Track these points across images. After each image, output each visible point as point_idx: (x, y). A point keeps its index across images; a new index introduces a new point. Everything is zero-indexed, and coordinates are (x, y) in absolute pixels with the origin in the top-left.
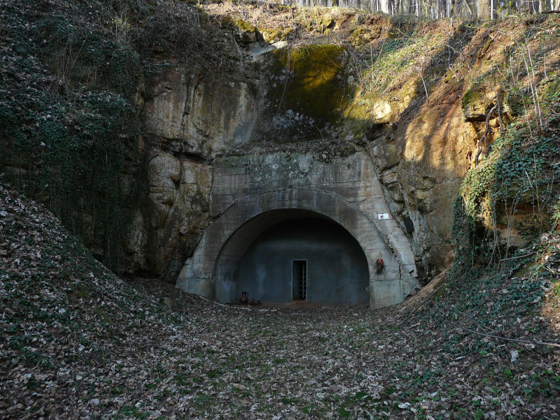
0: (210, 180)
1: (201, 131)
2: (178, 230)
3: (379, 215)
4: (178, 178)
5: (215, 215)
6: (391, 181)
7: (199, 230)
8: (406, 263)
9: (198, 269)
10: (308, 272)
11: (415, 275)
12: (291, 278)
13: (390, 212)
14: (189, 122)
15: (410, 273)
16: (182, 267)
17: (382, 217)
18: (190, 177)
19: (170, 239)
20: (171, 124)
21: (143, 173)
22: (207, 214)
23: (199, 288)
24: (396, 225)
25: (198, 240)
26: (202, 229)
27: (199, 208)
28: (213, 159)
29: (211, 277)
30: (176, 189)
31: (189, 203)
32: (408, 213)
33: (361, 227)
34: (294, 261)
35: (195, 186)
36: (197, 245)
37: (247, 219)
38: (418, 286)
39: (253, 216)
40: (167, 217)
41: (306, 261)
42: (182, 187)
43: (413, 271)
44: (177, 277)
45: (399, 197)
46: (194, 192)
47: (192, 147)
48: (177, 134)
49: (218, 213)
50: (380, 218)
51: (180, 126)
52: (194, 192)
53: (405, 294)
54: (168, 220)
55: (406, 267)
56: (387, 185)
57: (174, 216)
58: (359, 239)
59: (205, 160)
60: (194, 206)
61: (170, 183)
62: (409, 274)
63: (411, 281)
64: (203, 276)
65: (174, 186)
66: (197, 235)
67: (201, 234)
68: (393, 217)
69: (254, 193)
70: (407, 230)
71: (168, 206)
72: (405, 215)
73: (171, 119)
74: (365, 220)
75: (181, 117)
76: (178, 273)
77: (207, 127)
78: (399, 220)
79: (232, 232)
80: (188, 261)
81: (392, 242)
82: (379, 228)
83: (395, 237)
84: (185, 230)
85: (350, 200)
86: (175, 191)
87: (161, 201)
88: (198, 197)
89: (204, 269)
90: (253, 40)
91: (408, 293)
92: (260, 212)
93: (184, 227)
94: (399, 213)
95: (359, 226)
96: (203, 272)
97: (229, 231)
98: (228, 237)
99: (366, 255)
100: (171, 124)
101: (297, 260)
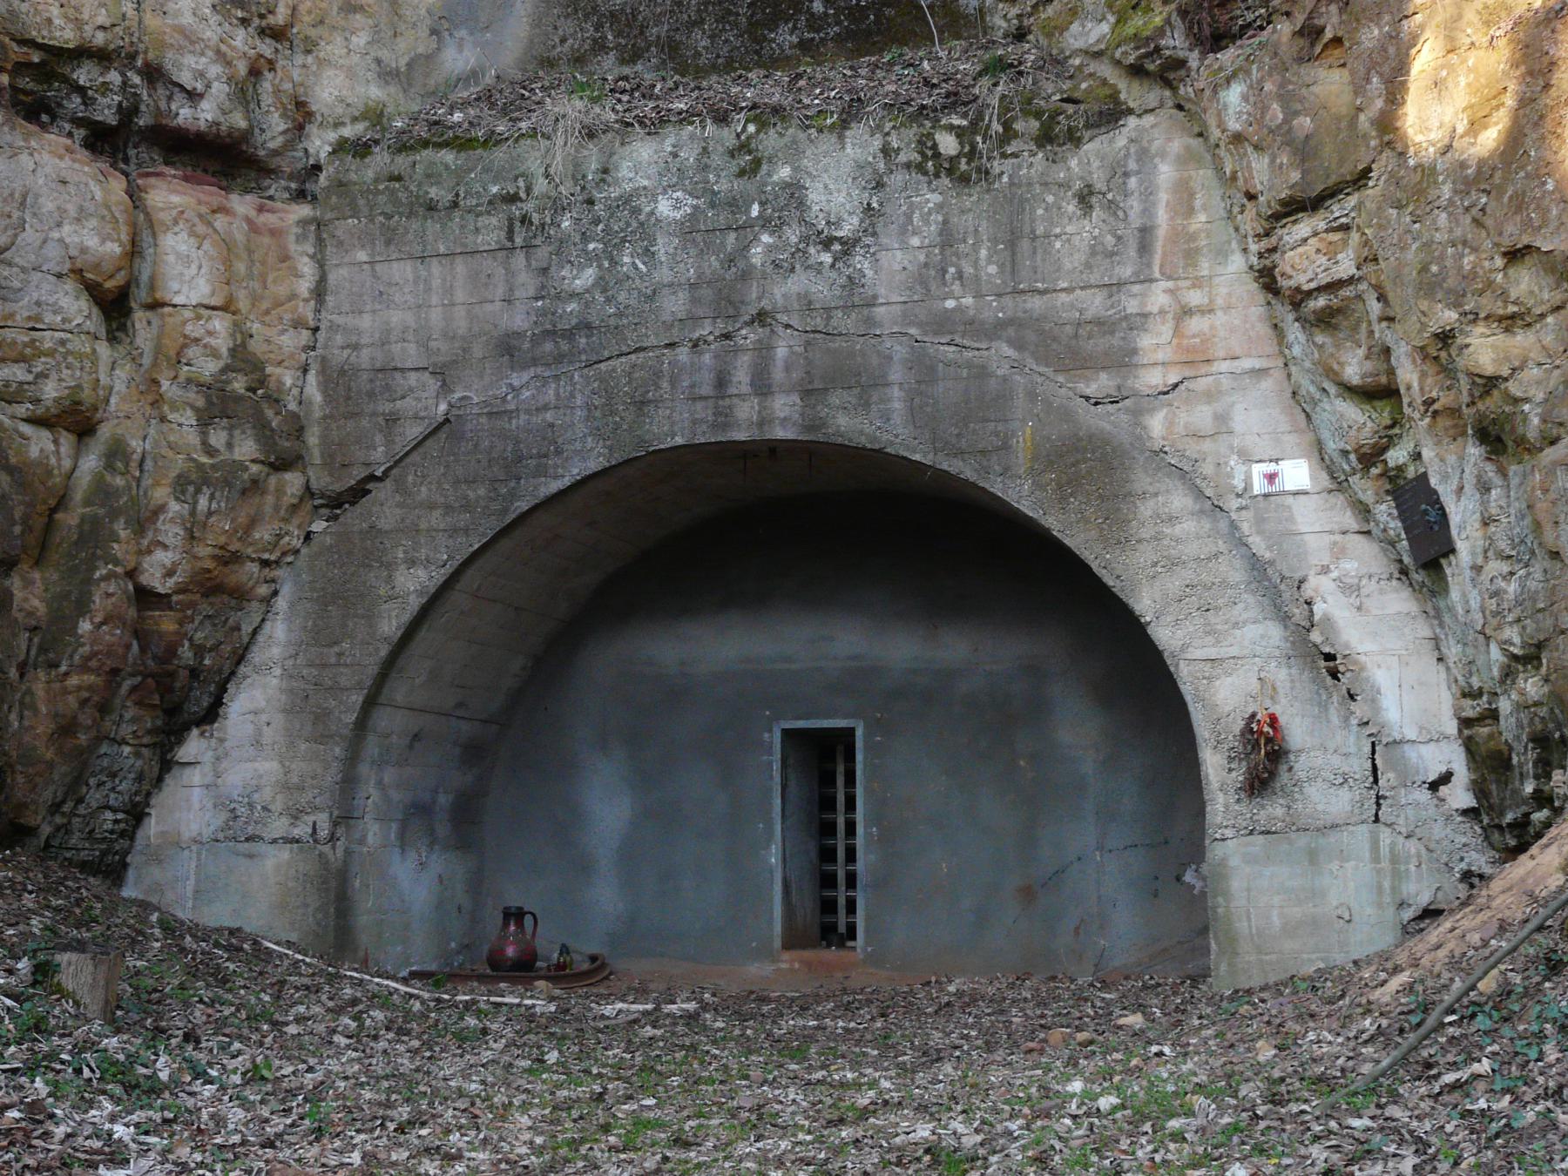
0: (304, 286)
2: (131, 574)
3: (1258, 470)
5: (338, 487)
7: (254, 568)
8: (1411, 734)
11: (1460, 796)
15: (1434, 786)
17: (1271, 478)
18: (186, 270)
19: (85, 626)
22: (293, 482)
24: (1349, 520)
25: (247, 629)
26: (265, 563)
28: (317, 168)
29: (323, 833)
30: (112, 339)
32: (1417, 456)
33: (1157, 538)
34: (786, 733)
35: (220, 324)
36: (240, 657)
37: (523, 505)
38: (1479, 860)
39: (555, 486)
40: (62, 502)
41: (850, 732)
43: (1446, 778)
44: (129, 834)
45: (1369, 366)
46: (215, 354)
47: (193, 96)
48: (102, 19)
49: (359, 473)
50: (1259, 486)
52: (215, 354)
53: (1402, 905)
55: (1411, 753)
57: (101, 491)
60: (217, 438)
61: (75, 306)
62: (1424, 795)
63: (1438, 831)
64: (279, 826)
65: (95, 323)
66: (240, 596)
69: (559, 358)
71: (67, 440)
72: (1400, 469)
76: (137, 814)
78: (1368, 497)
80: (193, 746)
81: (1327, 619)
82: (1258, 544)
83: (1349, 588)
84: (170, 573)
85: (1091, 390)
86: (103, 349)
87: (22, 410)
88: (239, 385)
89: (286, 787)
91: (1424, 899)
92: (594, 464)
93: (163, 557)
94: (1370, 457)
95: (1145, 533)
96: (277, 806)
97: (421, 573)
99: (1186, 689)
101: (801, 724)
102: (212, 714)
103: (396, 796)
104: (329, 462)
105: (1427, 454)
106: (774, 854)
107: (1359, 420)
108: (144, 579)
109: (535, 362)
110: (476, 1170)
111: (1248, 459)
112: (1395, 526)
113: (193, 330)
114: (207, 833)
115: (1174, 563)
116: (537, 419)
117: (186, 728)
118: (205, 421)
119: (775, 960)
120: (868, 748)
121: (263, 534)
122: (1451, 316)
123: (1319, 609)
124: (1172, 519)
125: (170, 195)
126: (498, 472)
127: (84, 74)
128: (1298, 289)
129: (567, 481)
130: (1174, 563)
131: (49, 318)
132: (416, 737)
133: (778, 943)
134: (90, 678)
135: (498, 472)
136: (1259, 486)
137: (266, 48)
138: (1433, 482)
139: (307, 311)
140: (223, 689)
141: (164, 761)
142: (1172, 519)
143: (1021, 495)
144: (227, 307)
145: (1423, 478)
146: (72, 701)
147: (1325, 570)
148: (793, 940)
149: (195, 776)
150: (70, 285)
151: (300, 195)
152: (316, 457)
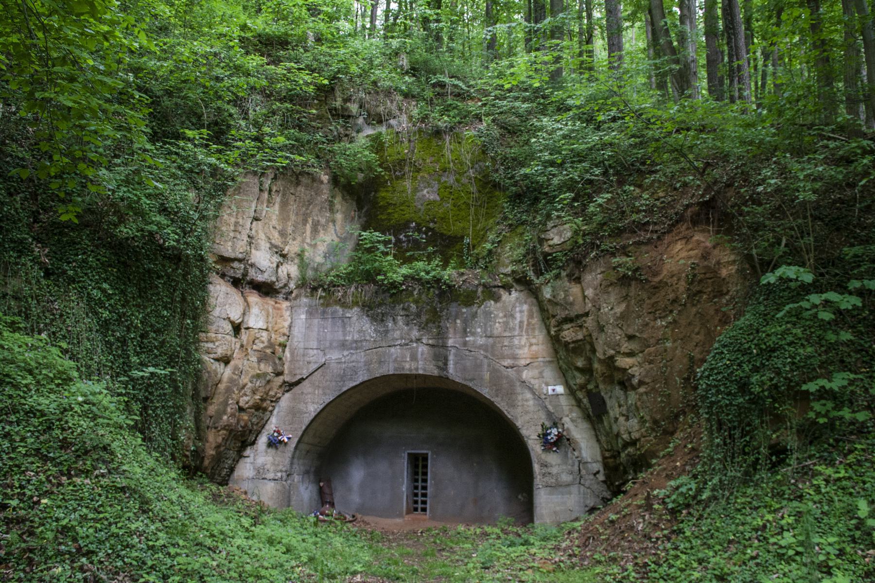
0: (286, 324)
1: (276, 247)
2: (237, 403)
3: (550, 388)
4: (240, 320)
5: (294, 381)
6: (574, 339)
7: (269, 402)
8: (589, 460)
9: (264, 465)
10: (431, 471)
11: (601, 477)
12: (403, 478)
13: (567, 385)
14: (260, 232)
15: (595, 475)
16: (238, 461)
17: (554, 390)
18: (256, 320)
19: (225, 417)
20: (232, 234)
21: (193, 311)
22: (280, 379)
23: (268, 492)
24: (574, 402)
25: (265, 419)
26: (272, 401)
27: (270, 369)
28: (292, 292)
29: (284, 478)
30: (236, 337)
31: (254, 359)
32: (597, 387)
33: (523, 405)
34: (427, 454)
35: (265, 334)
36: (263, 427)
37: (345, 389)
38: (607, 495)
39: (355, 384)
40: (220, 381)
41: (427, 454)
42: (244, 336)
43: (598, 472)
44: (229, 476)
45: (584, 363)
46: (263, 342)
47: (262, 272)
48: (241, 251)
49: (298, 377)
50: (550, 392)
51: (246, 238)
52: (263, 342)
53: (586, 506)
54: (222, 387)
55: (589, 466)
56: (567, 344)
57: (231, 380)
58: (519, 424)
59: (278, 293)
60: (262, 365)
61: (229, 328)
62: (592, 477)
63: (596, 486)
64: (271, 475)
65: (232, 333)
66: (265, 410)
67: (270, 408)
68: (571, 392)
69: (357, 349)
70: (593, 412)
71: (223, 365)
72: (591, 390)
73: (232, 228)
74: (529, 395)
75: (248, 225)
76: (232, 470)
77: (286, 243)
78: (581, 397)
79: (321, 407)
80: (248, 452)
81: (568, 429)
82: (550, 408)
83: (572, 421)
84: (247, 403)
85: (506, 364)
86: (233, 339)
87: (212, 356)
88: (269, 351)
89: (273, 464)
90: (355, 114)
91: (592, 505)
92: (366, 379)
93: (246, 399)
94: (582, 387)
95: (520, 404)
96: (271, 470)
97: (316, 406)
98: (313, 415)
99: (530, 448)
100: (232, 234)
101: (413, 451)
102: (253, 443)
103: (302, 468)
104: (290, 373)
105: (601, 386)
106: (404, 488)
107: (580, 379)
108: (241, 404)
109: (352, 349)
110: (79, 580)
111: (547, 385)
112: (588, 405)
113: (258, 335)
114: (251, 476)
115: (527, 412)
116: (351, 365)
117: (247, 446)
118: (260, 361)
119: (403, 517)
120: (432, 458)
121: (272, 393)
122: (612, 352)
123: (566, 426)
124: (527, 400)
125: (254, 298)
126: (338, 379)
127: (236, 265)
128: (567, 341)
129: (358, 383)
130: (527, 412)
131: (221, 330)
132: (308, 452)
133: (404, 513)
134: (225, 432)
135: (338, 379)
136: (550, 392)
137: (281, 259)
138: (602, 394)
139: (286, 331)
140: (257, 436)
141: (240, 456)
142: (527, 400)
143: (486, 392)
144: (267, 330)
145: (599, 392)
146: (221, 438)
147: (568, 416)
148: (408, 512)
149: (248, 460)
150: (227, 321)
151: (287, 299)
152: (286, 372)
